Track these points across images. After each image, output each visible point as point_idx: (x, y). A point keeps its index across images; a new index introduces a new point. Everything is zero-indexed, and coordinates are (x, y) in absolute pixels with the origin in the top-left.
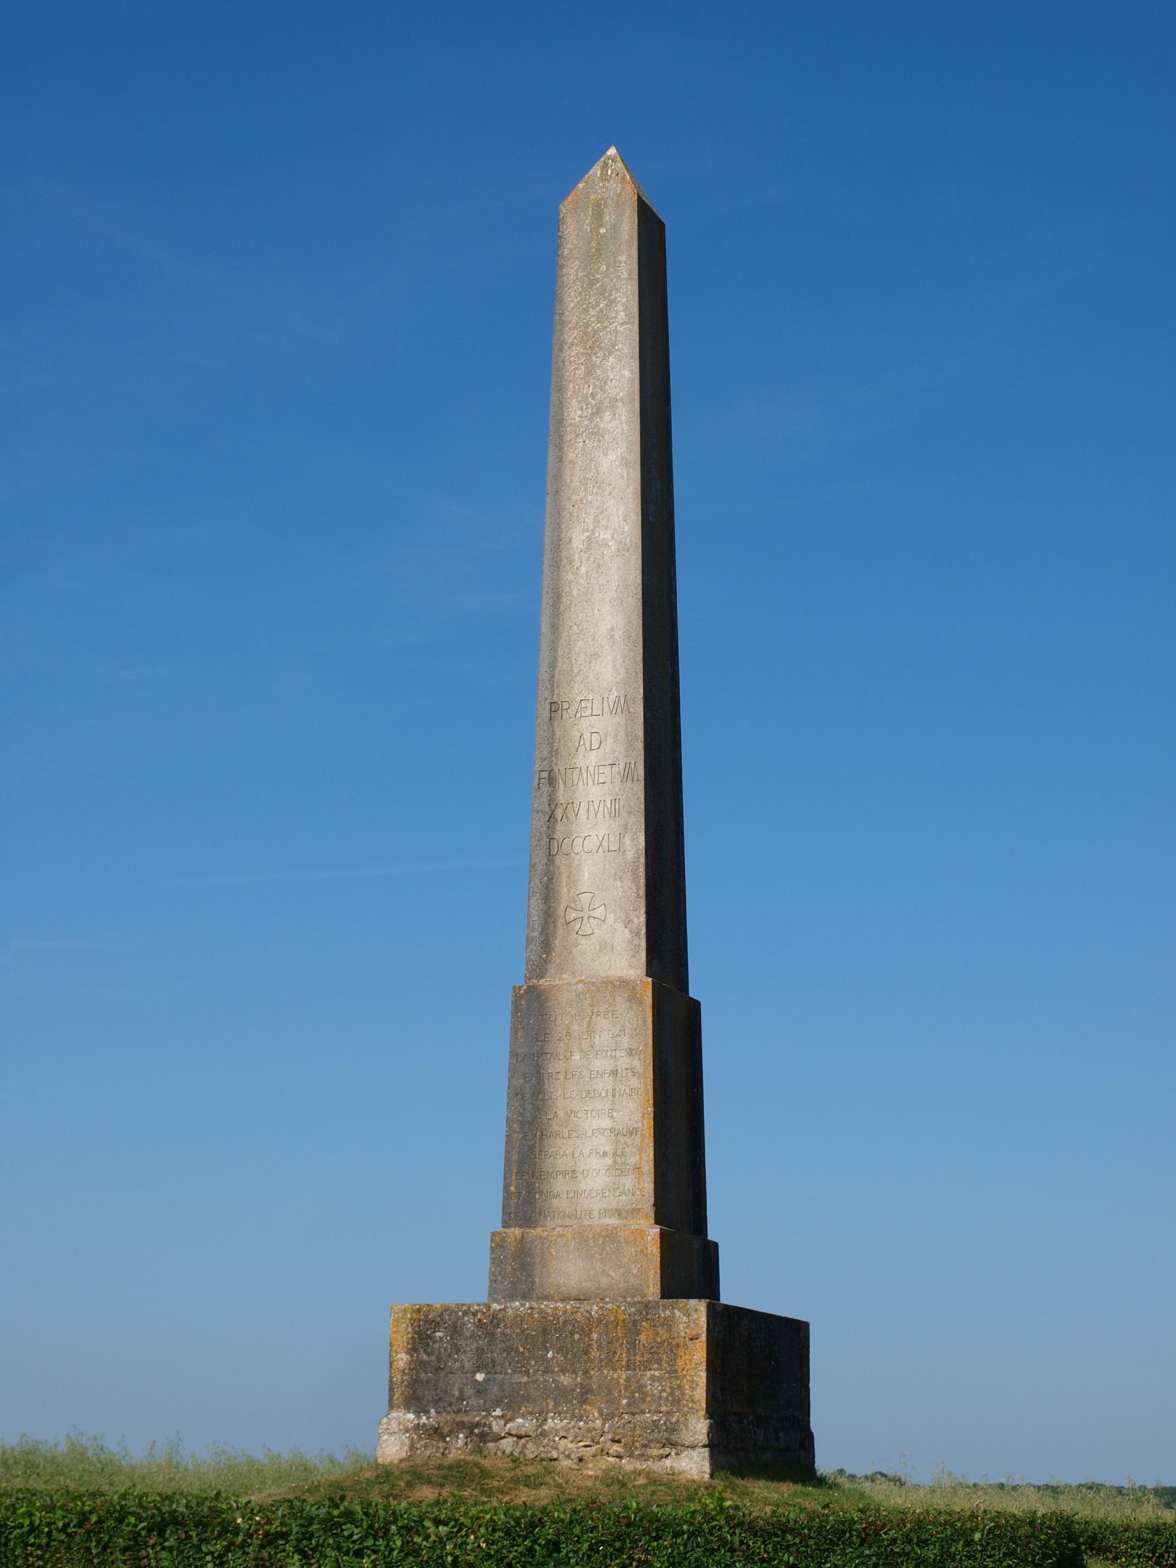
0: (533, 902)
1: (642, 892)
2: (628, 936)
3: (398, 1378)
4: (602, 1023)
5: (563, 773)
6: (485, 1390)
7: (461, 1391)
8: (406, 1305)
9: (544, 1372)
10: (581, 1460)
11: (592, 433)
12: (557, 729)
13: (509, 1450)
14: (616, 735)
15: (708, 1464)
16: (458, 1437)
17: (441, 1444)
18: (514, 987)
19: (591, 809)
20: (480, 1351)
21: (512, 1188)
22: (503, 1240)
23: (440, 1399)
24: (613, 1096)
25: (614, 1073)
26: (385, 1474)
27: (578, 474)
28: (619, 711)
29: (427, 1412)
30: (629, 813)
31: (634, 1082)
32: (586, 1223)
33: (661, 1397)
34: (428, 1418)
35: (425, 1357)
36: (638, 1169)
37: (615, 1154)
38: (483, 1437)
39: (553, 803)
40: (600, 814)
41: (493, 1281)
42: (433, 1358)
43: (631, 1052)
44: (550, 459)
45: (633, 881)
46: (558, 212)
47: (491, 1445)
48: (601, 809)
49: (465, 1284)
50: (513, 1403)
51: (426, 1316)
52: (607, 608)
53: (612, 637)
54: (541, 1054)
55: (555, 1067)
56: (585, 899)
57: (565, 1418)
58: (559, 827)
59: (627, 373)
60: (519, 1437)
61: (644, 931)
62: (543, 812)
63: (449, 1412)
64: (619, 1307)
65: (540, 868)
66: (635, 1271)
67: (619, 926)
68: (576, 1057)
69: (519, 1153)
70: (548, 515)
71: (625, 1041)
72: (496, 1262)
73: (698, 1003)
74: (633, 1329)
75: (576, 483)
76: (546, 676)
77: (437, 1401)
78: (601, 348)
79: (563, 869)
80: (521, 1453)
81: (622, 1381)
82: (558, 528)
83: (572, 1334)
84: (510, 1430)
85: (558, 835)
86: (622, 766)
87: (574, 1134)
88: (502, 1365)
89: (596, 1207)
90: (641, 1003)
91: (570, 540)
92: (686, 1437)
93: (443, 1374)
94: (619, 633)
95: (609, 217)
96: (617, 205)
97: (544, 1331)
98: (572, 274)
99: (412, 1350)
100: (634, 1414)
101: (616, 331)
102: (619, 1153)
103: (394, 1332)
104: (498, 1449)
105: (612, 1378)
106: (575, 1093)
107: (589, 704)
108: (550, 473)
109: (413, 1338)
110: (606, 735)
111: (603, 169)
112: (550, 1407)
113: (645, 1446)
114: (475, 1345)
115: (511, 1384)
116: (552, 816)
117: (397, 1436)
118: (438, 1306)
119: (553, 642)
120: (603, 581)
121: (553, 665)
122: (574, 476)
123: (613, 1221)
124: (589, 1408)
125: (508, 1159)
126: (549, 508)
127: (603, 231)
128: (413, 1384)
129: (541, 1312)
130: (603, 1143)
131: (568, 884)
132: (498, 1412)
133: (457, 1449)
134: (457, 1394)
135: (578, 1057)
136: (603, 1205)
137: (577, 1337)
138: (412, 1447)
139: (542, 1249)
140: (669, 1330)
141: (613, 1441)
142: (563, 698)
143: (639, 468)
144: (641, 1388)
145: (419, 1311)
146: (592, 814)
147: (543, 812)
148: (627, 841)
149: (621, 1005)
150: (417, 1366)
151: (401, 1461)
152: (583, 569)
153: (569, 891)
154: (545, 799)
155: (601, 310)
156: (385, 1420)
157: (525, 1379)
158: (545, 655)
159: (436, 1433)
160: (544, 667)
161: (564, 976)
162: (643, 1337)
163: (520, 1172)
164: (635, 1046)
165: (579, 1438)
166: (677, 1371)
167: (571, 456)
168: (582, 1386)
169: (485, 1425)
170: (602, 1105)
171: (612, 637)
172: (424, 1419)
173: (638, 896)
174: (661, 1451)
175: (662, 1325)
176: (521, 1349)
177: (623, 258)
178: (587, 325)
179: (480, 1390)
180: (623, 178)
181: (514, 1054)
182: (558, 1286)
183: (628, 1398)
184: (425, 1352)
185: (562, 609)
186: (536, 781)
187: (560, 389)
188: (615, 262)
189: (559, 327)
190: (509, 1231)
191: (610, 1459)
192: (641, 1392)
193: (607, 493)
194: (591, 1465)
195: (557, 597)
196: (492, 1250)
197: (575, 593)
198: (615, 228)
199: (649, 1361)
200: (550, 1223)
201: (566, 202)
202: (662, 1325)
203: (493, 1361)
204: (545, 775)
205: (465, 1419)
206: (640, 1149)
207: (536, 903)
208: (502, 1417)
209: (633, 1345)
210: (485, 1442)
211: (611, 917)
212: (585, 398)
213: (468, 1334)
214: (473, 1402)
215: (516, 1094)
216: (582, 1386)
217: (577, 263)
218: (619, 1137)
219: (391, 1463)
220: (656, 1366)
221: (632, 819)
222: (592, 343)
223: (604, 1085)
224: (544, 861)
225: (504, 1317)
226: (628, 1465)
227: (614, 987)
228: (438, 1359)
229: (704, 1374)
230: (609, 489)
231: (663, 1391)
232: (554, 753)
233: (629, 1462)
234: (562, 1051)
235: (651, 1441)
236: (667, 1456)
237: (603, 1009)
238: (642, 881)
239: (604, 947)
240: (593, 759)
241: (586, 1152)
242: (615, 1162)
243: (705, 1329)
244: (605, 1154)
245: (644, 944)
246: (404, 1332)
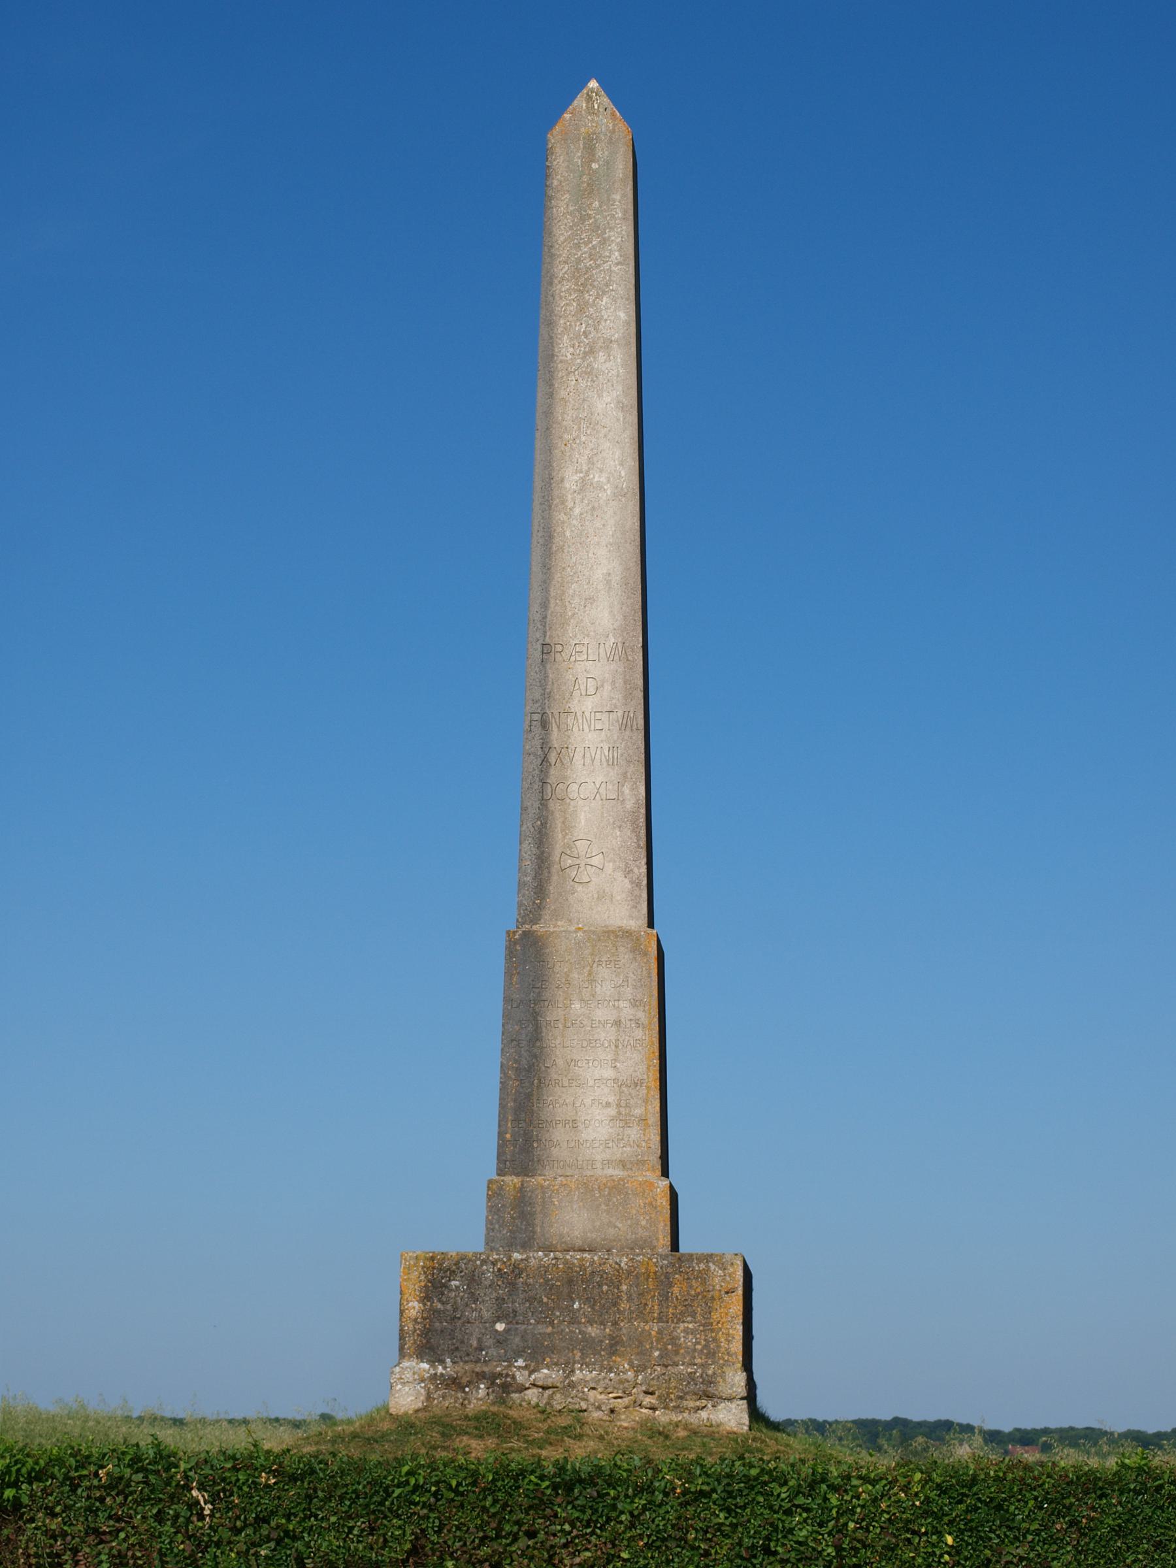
0: (525, 845)
2: (628, 885)
3: (409, 1327)
4: (603, 972)
5: (557, 716)
6: (506, 1340)
7: (479, 1340)
8: (418, 1253)
9: (569, 1323)
10: (612, 1411)
11: (585, 373)
12: (549, 671)
13: (534, 1401)
14: (613, 683)
15: (747, 1416)
16: (479, 1388)
17: (460, 1395)
18: (508, 932)
19: (587, 755)
20: (500, 1301)
21: (508, 1136)
22: (501, 1188)
23: (457, 1349)
24: (617, 1047)
25: (617, 1023)
26: (406, 1426)
27: (571, 412)
28: (617, 658)
29: (442, 1362)
31: (639, 1033)
32: (589, 1173)
33: (695, 1350)
34: (445, 1368)
35: (439, 1306)
36: (643, 1120)
37: (619, 1106)
38: (506, 1388)
39: (546, 746)
40: (597, 762)
41: (490, 1228)
42: (449, 1307)
43: (635, 1003)
44: (539, 395)
45: (633, 831)
46: (545, 142)
47: (515, 1396)
48: (598, 756)
49: (465, 1233)
50: (537, 1354)
51: (441, 1265)
52: (602, 552)
53: (608, 582)
54: (539, 1000)
55: (553, 1014)
57: (594, 1369)
58: (552, 771)
59: (622, 315)
60: (544, 1388)
62: (535, 755)
63: (466, 1362)
64: (650, 1259)
65: (532, 812)
66: (643, 1223)
67: (619, 875)
68: (577, 1006)
69: (515, 1101)
70: (537, 452)
72: (493, 1209)
75: (568, 422)
76: (537, 617)
77: (453, 1351)
78: (594, 287)
79: (557, 815)
80: (548, 1403)
81: (653, 1333)
82: (548, 465)
83: (600, 1285)
84: (536, 1383)
85: (552, 780)
86: (620, 714)
87: (575, 1083)
88: (525, 1315)
90: (645, 954)
91: (562, 480)
92: (724, 1389)
93: (459, 1323)
94: (616, 579)
95: (602, 152)
96: (610, 142)
97: (570, 1282)
98: (562, 206)
99: (426, 1298)
100: (666, 1366)
101: (610, 270)
102: (623, 1103)
103: (405, 1280)
104: (524, 1400)
105: (643, 1330)
106: (575, 1042)
107: (585, 649)
108: (540, 411)
109: (426, 1286)
110: (603, 682)
111: (588, 102)
112: (577, 1358)
113: (681, 1398)
114: (494, 1295)
115: (534, 1335)
116: (545, 759)
117: (412, 1386)
118: (454, 1254)
119: (545, 582)
120: (598, 524)
121: (545, 605)
122: (566, 415)
123: (618, 1173)
124: (619, 1359)
125: (502, 1106)
126: (538, 445)
127: (595, 166)
128: (427, 1333)
129: (566, 1262)
132: (520, 1363)
133: (478, 1399)
134: (475, 1344)
135: (578, 1006)
137: (605, 1288)
138: (429, 1397)
139: (543, 1198)
140: (704, 1282)
141: (646, 1393)
142: (556, 640)
144: (674, 1340)
145: (432, 1259)
146: (588, 761)
147: (535, 755)
148: (626, 790)
149: (625, 956)
150: (431, 1315)
151: (417, 1411)
152: (577, 511)
153: (564, 837)
154: (537, 742)
155: (594, 247)
156: (397, 1369)
157: (550, 1330)
158: (536, 594)
159: (454, 1383)
160: (535, 607)
161: (559, 923)
162: (676, 1290)
163: (516, 1120)
164: (639, 997)
165: (609, 1390)
167: (563, 394)
168: (611, 1338)
169: (507, 1375)
170: (606, 1055)
171: (608, 582)
172: (440, 1369)
173: (639, 846)
174: (698, 1403)
175: (697, 1278)
176: (545, 1300)
178: (579, 261)
179: (501, 1340)
180: (613, 114)
181: (508, 1000)
182: (562, 1236)
183: (660, 1350)
184: (440, 1300)
185: (554, 549)
186: (528, 722)
187: (551, 324)
188: (609, 200)
189: (548, 260)
190: (508, 1179)
191: (643, 1410)
192: (674, 1344)
193: (601, 435)
194: (623, 1417)
195: (549, 538)
196: (489, 1198)
197: (568, 534)
198: (608, 164)
199: (682, 1313)
200: (549, 1173)
201: (555, 132)
202: (697, 1278)
203: (515, 1311)
204: (536, 717)
205: (486, 1369)
206: (646, 1101)
207: (529, 847)
208: (526, 1367)
209: (665, 1297)
210: (508, 1393)
212: (577, 336)
213: (487, 1283)
214: (493, 1352)
215: (510, 1040)
216: (611, 1338)
217: (567, 196)
219: (406, 1414)
220: (689, 1319)
221: (631, 769)
222: (584, 280)
223: (606, 1034)
224: (537, 804)
225: (527, 1267)
226: (663, 1417)
227: (617, 936)
228: (447, 1310)
230: (604, 431)
231: (698, 1343)
232: (547, 696)
233: (664, 1414)
234: (561, 999)
235: (687, 1393)
239: (601, 896)
240: (589, 705)
241: (588, 1101)
242: (620, 1113)
244: (608, 1105)
246: (416, 1281)
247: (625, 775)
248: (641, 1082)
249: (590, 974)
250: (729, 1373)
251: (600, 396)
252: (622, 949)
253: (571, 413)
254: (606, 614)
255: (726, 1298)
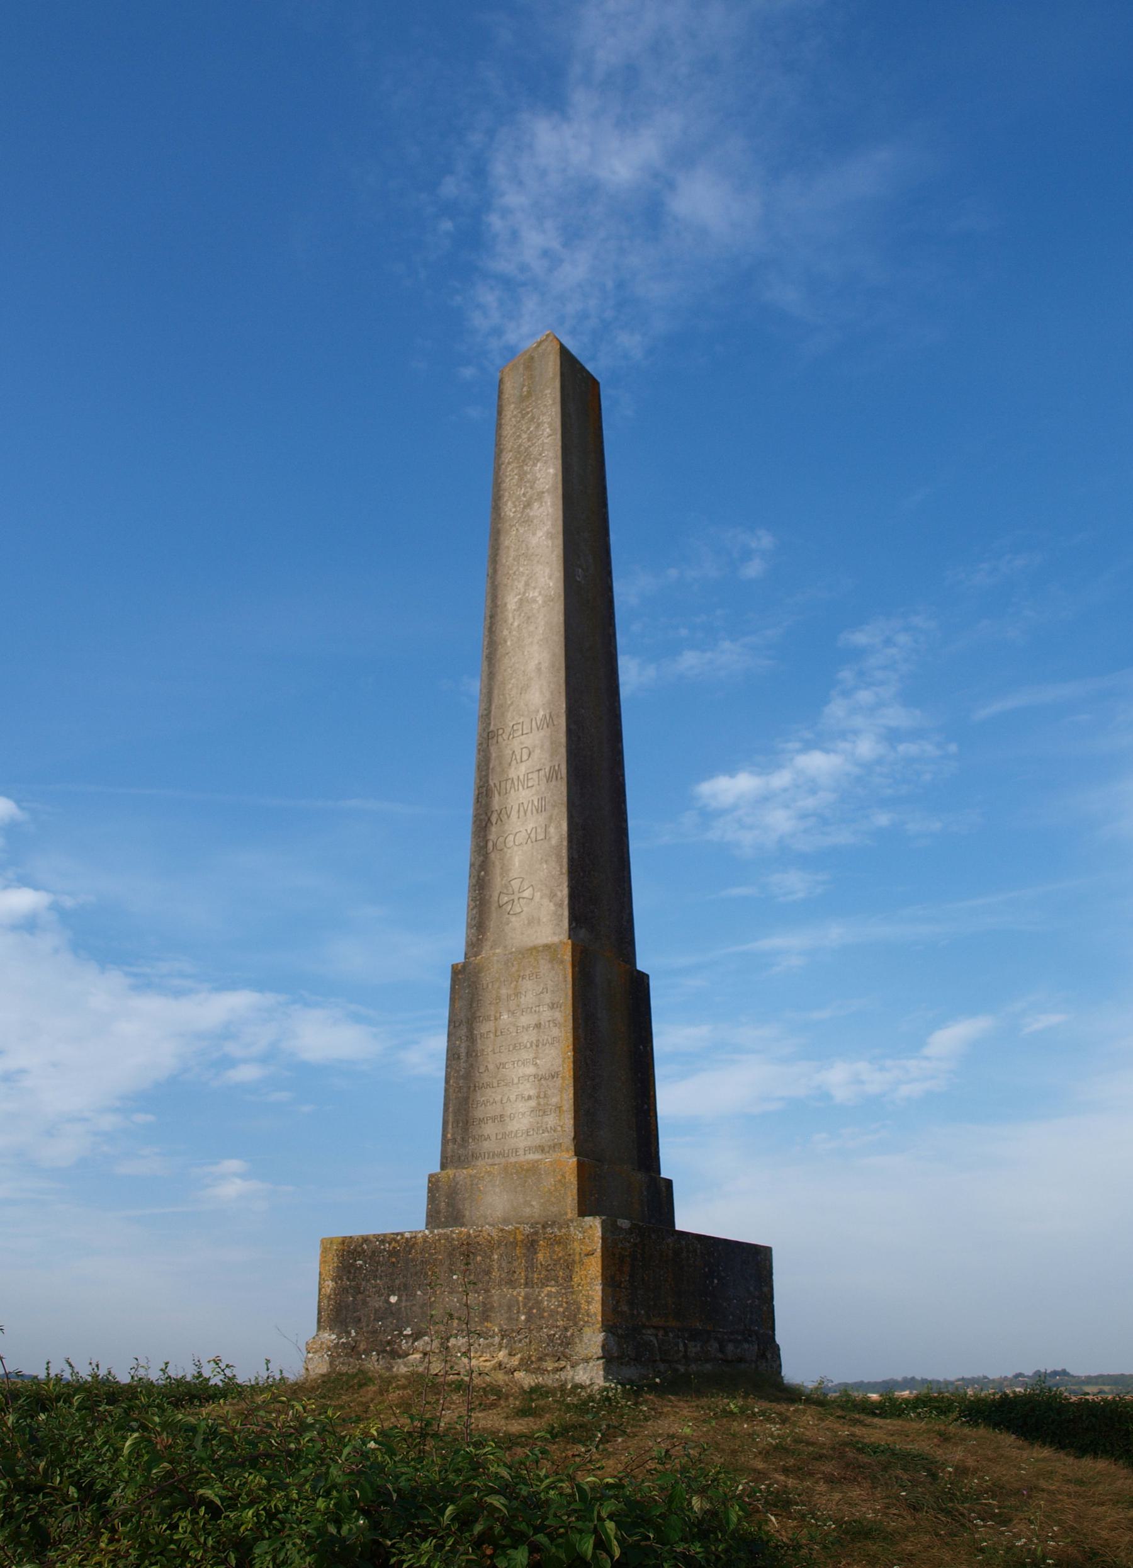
1: (565, 870)
14: (542, 746)
25: (538, 1026)
30: (554, 806)
31: (555, 1032)
32: (512, 1160)
36: (559, 1108)
52: (536, 647)
56: (515, 884)
59: (551, 471)
61: (566, 902)
67: (546, 902)
71: (547, 998)
73: (648, 976)
74: (531, 1245)
79: (497, 863)
86: (547, 770)
89: (522, 1145)
90: (562, 962)
94: (545, 665)
120: (532, 628)
124: (489, 1325)
130: (528, 1089)
131: (501, 874)
136: (529, 1142)
143: (561, 536)
144: (539, 1303)
146: (522, 813)
148: (552, 830)
149: (544, 966)
152: (516, 624)
162: (540, 1256)
164: (556, 1000)
166: (572, 1287)
167: (507, 543)
171: (539, 670)
173: (562, 873)
174: (556, 1365)
177: (548, 391)
184: (348, 1279)
192: (539, 1309)
206: (561, 1091)
211: (538, 895)
212: (518, 498)
218: (543, 1081)
221: (556, 811)
222: (525, 457)
229: (599, 1288)
235: (547, 1355)
236: (561, 1369)
237: (528, 972)
238: (565, 861)
239: (532, 921)
241: (513, 1098)
242: (539, 1104)
243: (600, 1245)
244: (530, 1098)
245: (566, 913)
247: (551, 818)
248: (557, 1074)
249: (515, 988)
250: (587, 1331)
251: (534, 534)
252: (542, 962)
253: (512, 554)
254: (537, 694)
255: (586, 1260)
